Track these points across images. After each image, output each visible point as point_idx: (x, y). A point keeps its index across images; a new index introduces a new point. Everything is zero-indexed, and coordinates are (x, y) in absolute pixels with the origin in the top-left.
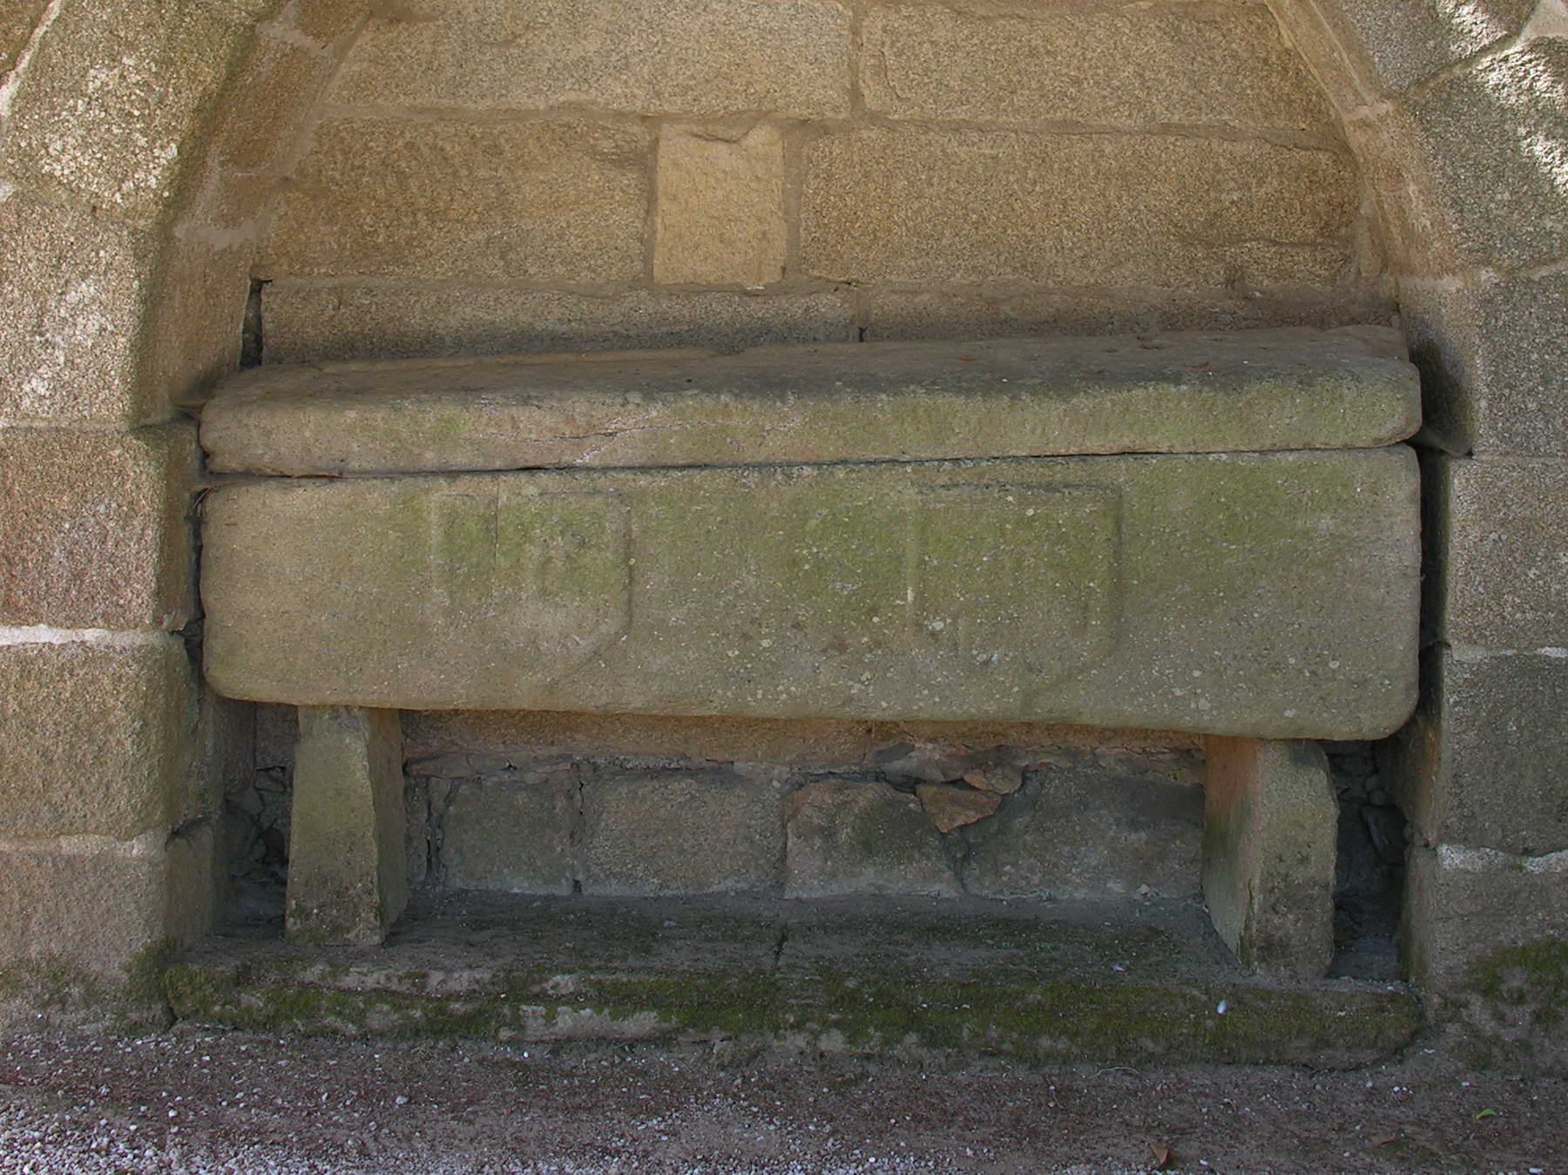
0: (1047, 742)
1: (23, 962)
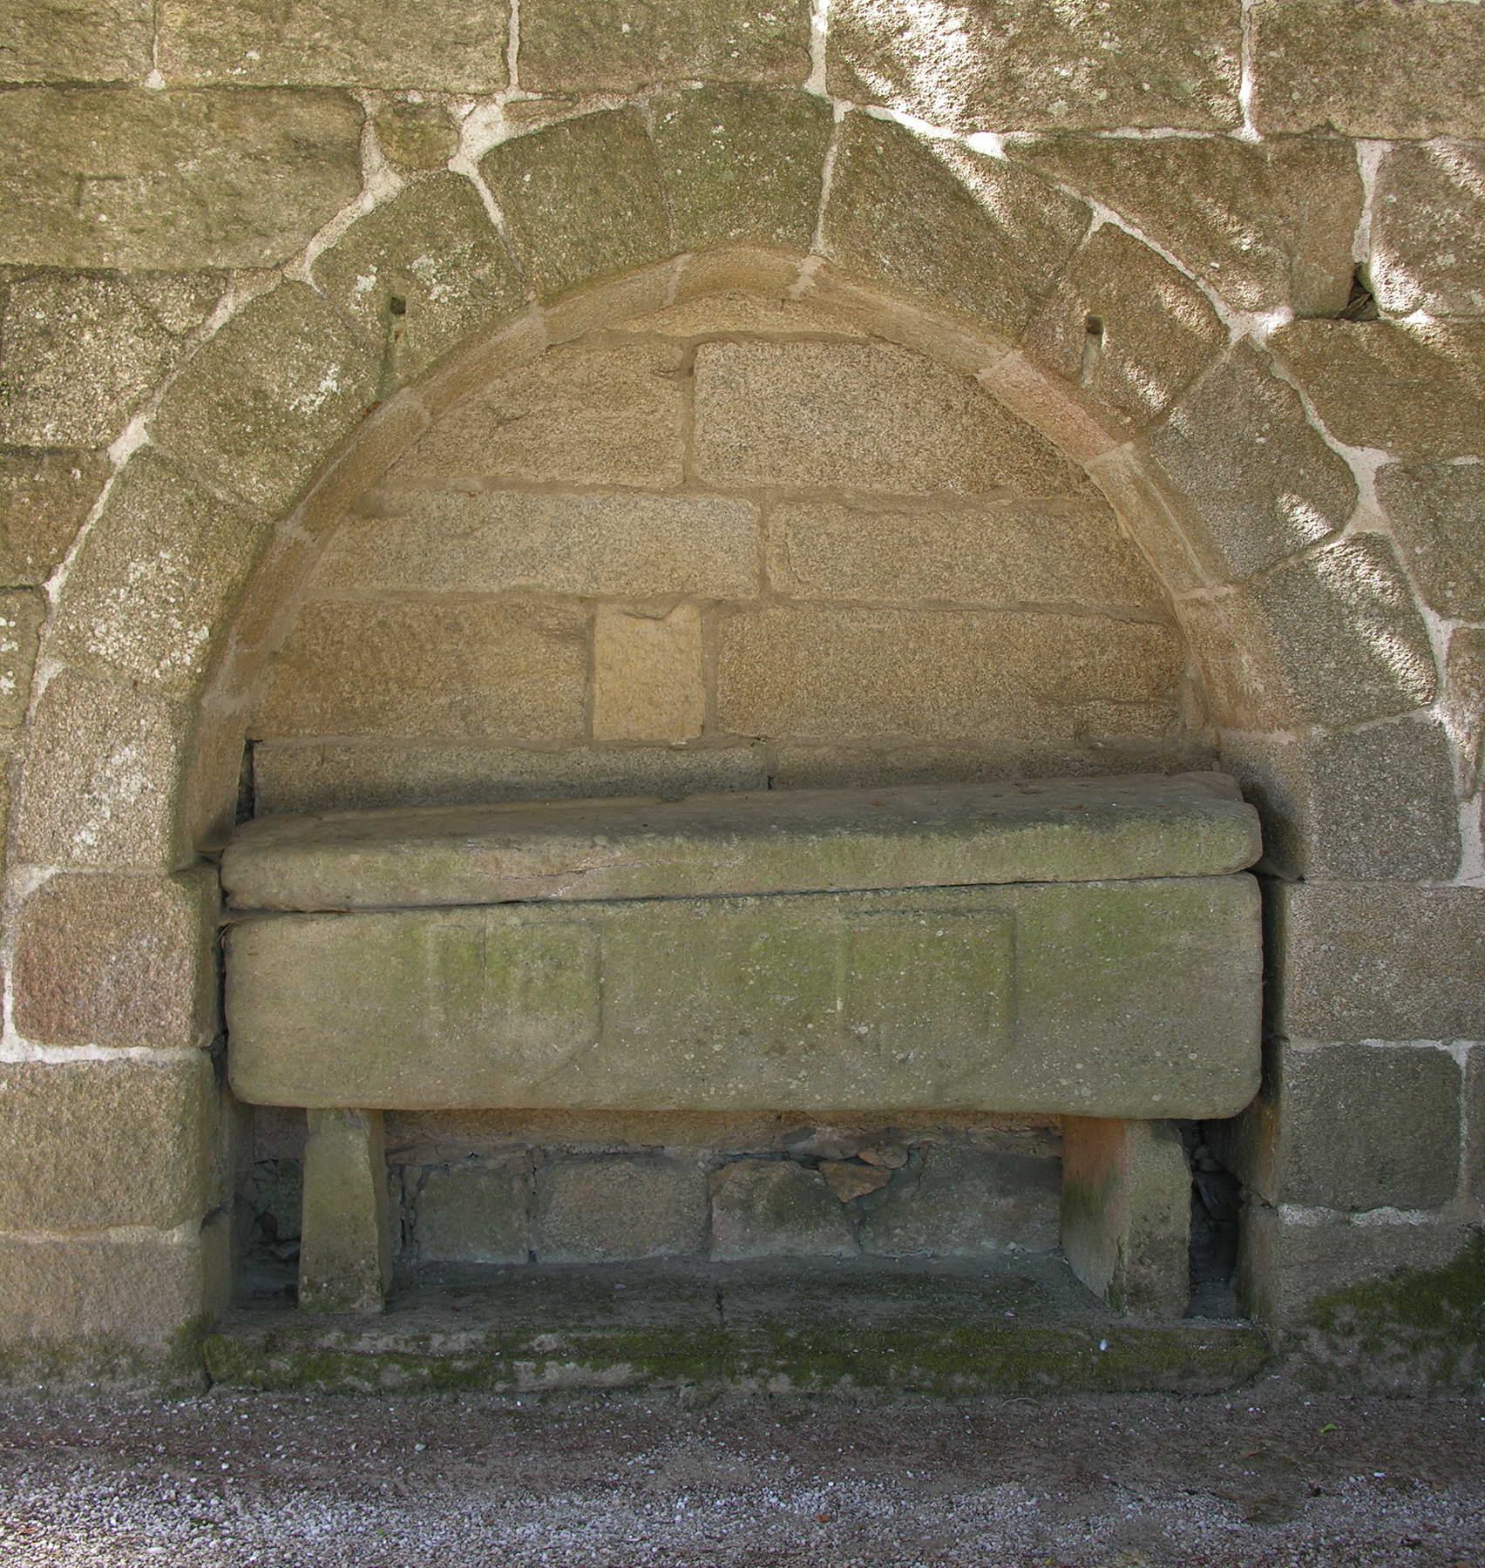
0: (929, 1124)
1: (78, 1338)
